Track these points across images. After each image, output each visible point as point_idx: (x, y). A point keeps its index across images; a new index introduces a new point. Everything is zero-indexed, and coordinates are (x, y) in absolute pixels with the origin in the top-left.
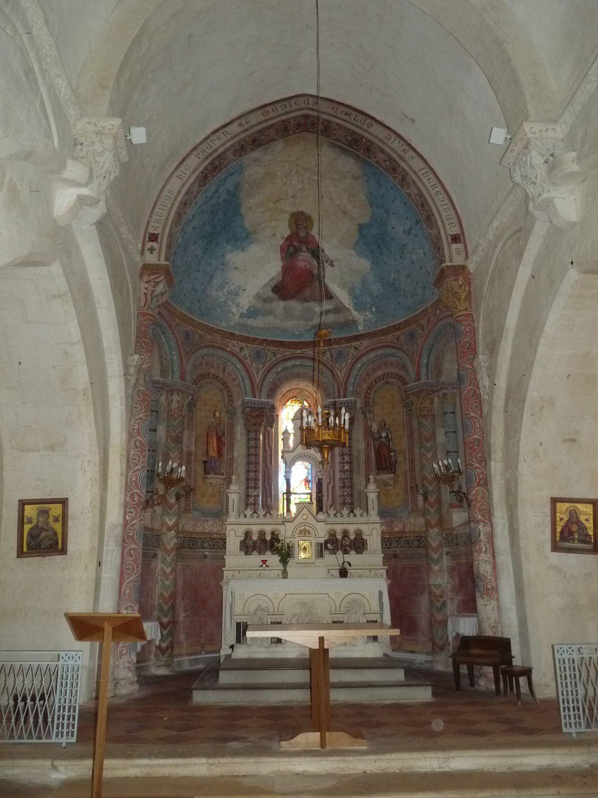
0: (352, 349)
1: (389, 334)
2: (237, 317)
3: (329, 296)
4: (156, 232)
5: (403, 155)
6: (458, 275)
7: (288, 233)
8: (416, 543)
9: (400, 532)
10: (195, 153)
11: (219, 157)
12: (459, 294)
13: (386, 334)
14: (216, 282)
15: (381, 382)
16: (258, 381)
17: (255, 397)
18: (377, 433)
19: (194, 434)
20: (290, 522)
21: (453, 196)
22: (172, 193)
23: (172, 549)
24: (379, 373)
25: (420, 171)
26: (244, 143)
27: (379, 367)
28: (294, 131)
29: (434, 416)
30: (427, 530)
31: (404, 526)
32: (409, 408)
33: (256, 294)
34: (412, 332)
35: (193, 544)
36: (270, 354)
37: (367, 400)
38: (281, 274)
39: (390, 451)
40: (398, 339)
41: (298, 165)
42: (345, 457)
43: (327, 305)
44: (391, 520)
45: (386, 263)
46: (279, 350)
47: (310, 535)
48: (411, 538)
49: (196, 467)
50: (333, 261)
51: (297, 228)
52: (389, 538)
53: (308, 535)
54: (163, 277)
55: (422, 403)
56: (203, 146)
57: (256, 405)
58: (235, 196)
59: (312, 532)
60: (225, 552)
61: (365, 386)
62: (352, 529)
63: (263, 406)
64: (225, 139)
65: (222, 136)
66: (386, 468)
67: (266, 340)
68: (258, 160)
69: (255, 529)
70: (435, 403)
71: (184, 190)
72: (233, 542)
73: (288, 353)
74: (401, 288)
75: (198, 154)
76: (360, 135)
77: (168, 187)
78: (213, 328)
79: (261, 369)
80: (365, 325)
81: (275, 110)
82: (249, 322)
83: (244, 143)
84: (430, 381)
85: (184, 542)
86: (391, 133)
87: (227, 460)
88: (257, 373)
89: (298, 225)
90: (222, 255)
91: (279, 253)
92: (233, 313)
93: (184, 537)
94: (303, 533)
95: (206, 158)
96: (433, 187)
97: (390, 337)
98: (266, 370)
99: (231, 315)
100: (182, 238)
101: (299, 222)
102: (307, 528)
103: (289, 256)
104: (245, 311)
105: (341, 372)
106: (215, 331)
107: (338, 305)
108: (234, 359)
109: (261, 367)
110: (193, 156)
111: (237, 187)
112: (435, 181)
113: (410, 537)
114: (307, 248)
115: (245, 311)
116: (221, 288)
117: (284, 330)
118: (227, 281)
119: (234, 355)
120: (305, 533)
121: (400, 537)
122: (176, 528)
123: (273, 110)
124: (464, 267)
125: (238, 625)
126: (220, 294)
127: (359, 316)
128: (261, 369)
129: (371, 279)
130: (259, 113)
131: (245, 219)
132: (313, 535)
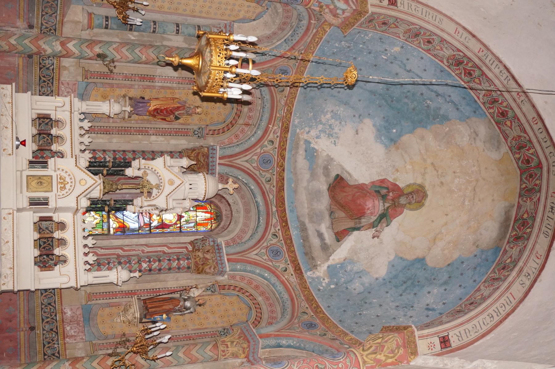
0: (284, 266)
1: (308, 303)
2: (305, 136)
3: (340, 236)
4: (399, 5)
5: (523, 274)
6: (404, 347)
7: (401, 185)
8: (49, 352)
9: (64, 331)
10: (483, 48)
11: (483, 73)
12: (382, 351)
13: (307, 300)
14: (341, 110)
15: (250, 303)
16: (238, 161)
17: (220, 158)
18: (189, 298)
19: (175, 85)
20: (76, 163)
21: (492, 335)
22: (441, 23)
23: (39, 47)
24: (260, 299)
25: (511, 293)
26: (500, 102)
27: (267, 299)
28: (519, 159)
29: (216, 360)
30: (68, 360)
31: (72, 336)
32: (222, 333)
33: (332, 157)
34: (315, 325)
35: (44, 81)
36: (268, 175)
37: (227, 287)
38: (357, 184)
39: (168, 312)
40: (304, 313)
41: (477, 181)
42: (157, 263)
43: (329, 237)
44: (80, 321)
45: (387, 292)
46: (274, 187)
47: (59, 190)
48: (56, 346)
49: (136, 87)
50: (378, 237)
51: (407, 194)
52: (56, 320)
53: (59, 186)
54: (354, 8)
55: (232, 342)
56: (490, 56)
57: (211, 160)
58: (434, 119)
59: (64, 192)
60: (35, 94)
61: (242, 285)
63: (210, 168)
64: (502, 79)
65: (505, 76)
66: (147, 308)
67: (284, 170)
68: (477, 135)
69: (67, 235)
70: (234, 360)
71: (445, 36)
73: (271, 197)
74: (362, 311)
75: (483, 51)
76: (533, 225)
77: (445, 19)
78: (293, 106)
79: (252, 165)
80: (313, 278)
81: (541, 131)
82: (301, 152)
83: (500, 102)
84: (261, 351)
85: (48, 69)
86: (543, 258)
87: (145, 128)
88: (247, 161)
89: (412, 194)
90: (369, 114)
91: (378, 179)
92: (309, 132)
93: (53, 69)
94: (62, 181)
95: (480, 59)
96: (497, 311)
97: (305, 304)
98: (251, 171)
99: (307, 129)
100: (386, 60)
101: (415, 194)
102: (68, 186)
103: (377, 189)
104: (312, 145)
105: (256, 254)
106: (289, 108)
107: (331, 249)
108: (260, 133)
109: (254, 165)
110: (479, 46)
111: (445, 118)
112: (503, 314)
113: (58, 344)
114: (388, 208)
115: (312, 145)
116: (335, 116)
117: (295, 192)
118: (343, 123)
119: (266, 131)
120: (62, 183)
121: (57, 333)
122: (65, 53)
123: (539, 129)
124: (415, 353)
126: (329, 116)
127: (322, 271)
128: (252, 165)
129: (366, 280)
130: (535, 115)
131: (410, 135)
132: (59, 193)
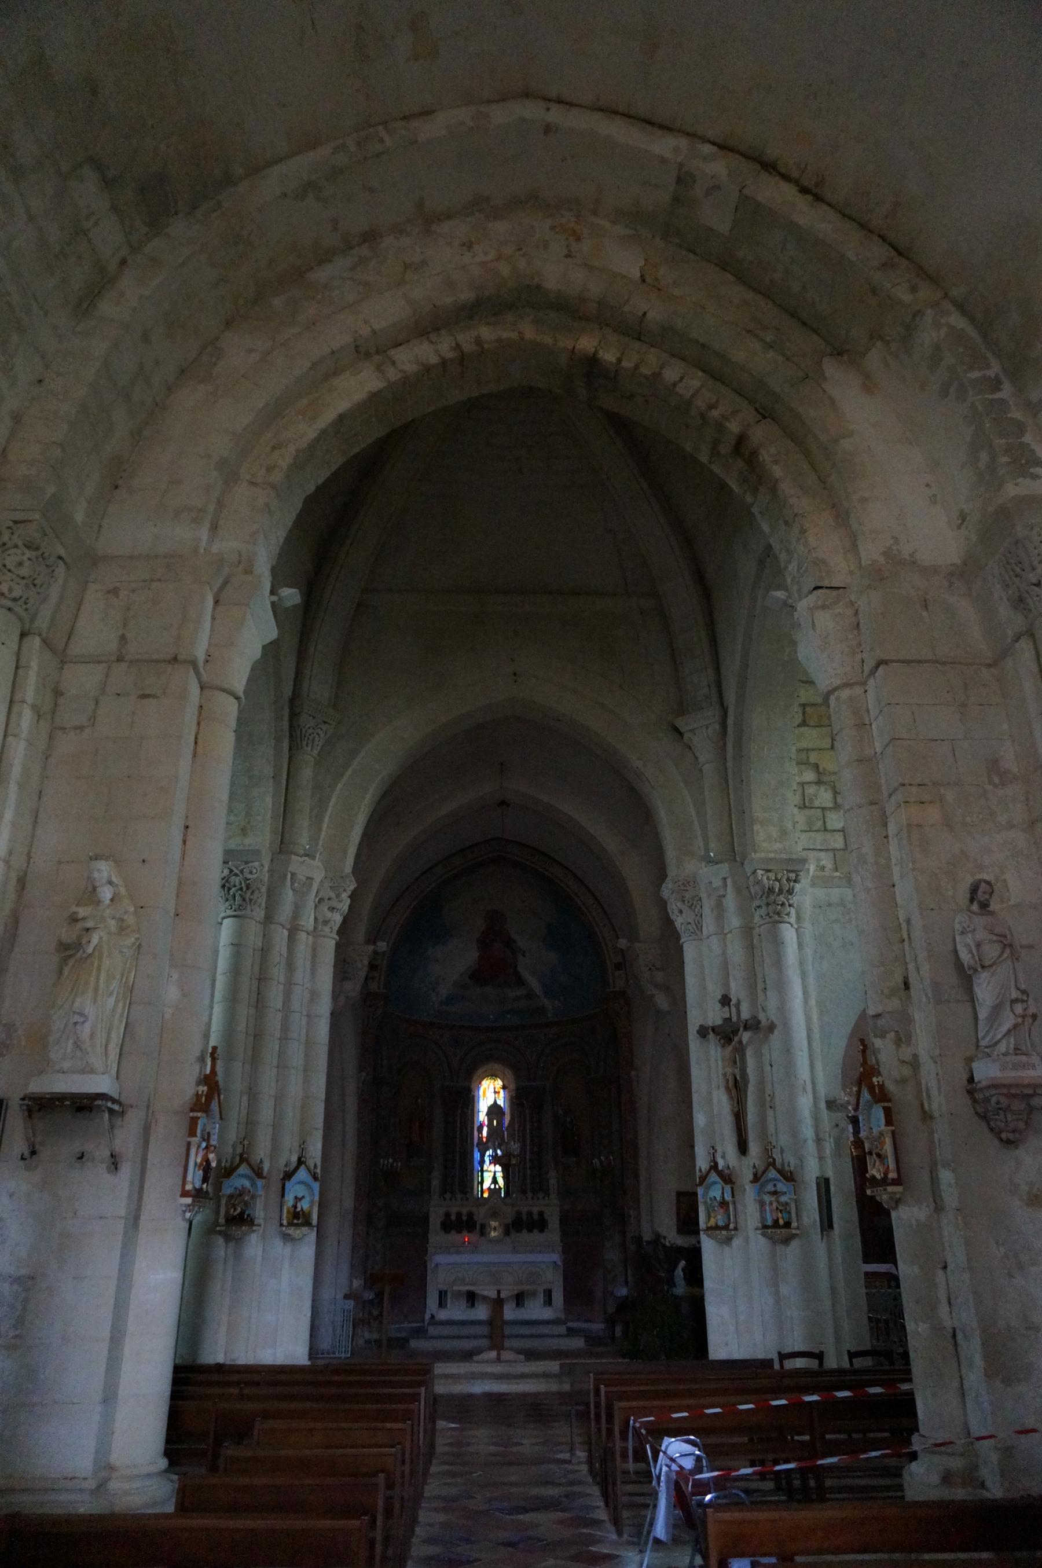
3: (521, 982)
62: (535, 1210)
69: (454, 1210)
72: (435, 1220)
125: (440, 1292)
